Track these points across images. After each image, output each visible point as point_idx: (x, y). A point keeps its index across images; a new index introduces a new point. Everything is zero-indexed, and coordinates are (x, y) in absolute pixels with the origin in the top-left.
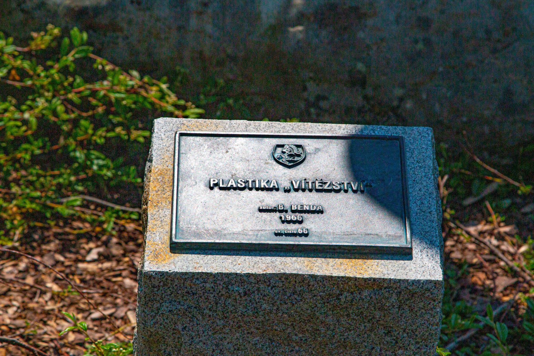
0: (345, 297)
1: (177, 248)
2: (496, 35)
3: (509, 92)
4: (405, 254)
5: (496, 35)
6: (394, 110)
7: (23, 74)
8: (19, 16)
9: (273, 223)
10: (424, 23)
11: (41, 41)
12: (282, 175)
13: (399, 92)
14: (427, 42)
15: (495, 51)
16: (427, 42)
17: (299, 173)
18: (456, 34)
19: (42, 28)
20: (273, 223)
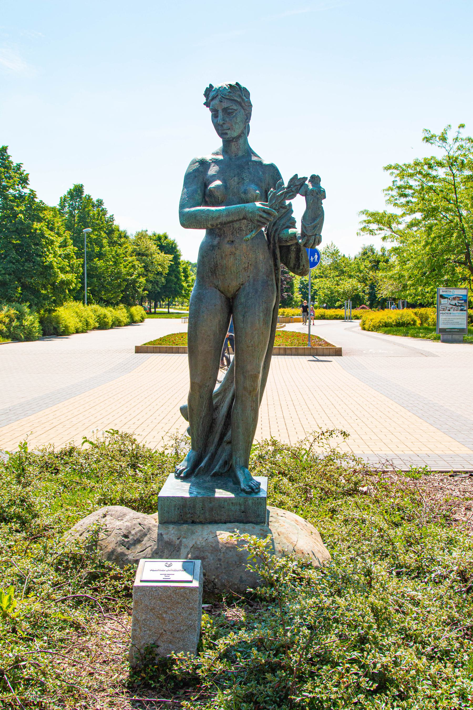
0: (178, 591)
1: (142, 581)
2: (238, 563)
3: (241, 577)
4: (191, 582)
5: (238, 563)
6: (213, 582)
7: (121, 574)
8: (122, 562)
9: (163, 576)
10: (220, 560)
11: (126, 567)
12: (167, 568)
13: (214, 577)
14: (220, 564)
15: (237, 567)
16: (220, 564)
17: (169, 568)
18: (227, 563)
19: (127, 565)
20: (163, 576)
